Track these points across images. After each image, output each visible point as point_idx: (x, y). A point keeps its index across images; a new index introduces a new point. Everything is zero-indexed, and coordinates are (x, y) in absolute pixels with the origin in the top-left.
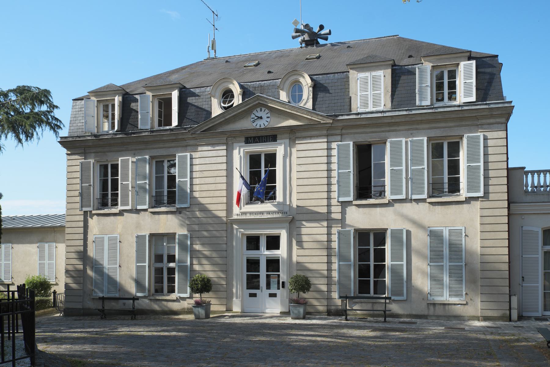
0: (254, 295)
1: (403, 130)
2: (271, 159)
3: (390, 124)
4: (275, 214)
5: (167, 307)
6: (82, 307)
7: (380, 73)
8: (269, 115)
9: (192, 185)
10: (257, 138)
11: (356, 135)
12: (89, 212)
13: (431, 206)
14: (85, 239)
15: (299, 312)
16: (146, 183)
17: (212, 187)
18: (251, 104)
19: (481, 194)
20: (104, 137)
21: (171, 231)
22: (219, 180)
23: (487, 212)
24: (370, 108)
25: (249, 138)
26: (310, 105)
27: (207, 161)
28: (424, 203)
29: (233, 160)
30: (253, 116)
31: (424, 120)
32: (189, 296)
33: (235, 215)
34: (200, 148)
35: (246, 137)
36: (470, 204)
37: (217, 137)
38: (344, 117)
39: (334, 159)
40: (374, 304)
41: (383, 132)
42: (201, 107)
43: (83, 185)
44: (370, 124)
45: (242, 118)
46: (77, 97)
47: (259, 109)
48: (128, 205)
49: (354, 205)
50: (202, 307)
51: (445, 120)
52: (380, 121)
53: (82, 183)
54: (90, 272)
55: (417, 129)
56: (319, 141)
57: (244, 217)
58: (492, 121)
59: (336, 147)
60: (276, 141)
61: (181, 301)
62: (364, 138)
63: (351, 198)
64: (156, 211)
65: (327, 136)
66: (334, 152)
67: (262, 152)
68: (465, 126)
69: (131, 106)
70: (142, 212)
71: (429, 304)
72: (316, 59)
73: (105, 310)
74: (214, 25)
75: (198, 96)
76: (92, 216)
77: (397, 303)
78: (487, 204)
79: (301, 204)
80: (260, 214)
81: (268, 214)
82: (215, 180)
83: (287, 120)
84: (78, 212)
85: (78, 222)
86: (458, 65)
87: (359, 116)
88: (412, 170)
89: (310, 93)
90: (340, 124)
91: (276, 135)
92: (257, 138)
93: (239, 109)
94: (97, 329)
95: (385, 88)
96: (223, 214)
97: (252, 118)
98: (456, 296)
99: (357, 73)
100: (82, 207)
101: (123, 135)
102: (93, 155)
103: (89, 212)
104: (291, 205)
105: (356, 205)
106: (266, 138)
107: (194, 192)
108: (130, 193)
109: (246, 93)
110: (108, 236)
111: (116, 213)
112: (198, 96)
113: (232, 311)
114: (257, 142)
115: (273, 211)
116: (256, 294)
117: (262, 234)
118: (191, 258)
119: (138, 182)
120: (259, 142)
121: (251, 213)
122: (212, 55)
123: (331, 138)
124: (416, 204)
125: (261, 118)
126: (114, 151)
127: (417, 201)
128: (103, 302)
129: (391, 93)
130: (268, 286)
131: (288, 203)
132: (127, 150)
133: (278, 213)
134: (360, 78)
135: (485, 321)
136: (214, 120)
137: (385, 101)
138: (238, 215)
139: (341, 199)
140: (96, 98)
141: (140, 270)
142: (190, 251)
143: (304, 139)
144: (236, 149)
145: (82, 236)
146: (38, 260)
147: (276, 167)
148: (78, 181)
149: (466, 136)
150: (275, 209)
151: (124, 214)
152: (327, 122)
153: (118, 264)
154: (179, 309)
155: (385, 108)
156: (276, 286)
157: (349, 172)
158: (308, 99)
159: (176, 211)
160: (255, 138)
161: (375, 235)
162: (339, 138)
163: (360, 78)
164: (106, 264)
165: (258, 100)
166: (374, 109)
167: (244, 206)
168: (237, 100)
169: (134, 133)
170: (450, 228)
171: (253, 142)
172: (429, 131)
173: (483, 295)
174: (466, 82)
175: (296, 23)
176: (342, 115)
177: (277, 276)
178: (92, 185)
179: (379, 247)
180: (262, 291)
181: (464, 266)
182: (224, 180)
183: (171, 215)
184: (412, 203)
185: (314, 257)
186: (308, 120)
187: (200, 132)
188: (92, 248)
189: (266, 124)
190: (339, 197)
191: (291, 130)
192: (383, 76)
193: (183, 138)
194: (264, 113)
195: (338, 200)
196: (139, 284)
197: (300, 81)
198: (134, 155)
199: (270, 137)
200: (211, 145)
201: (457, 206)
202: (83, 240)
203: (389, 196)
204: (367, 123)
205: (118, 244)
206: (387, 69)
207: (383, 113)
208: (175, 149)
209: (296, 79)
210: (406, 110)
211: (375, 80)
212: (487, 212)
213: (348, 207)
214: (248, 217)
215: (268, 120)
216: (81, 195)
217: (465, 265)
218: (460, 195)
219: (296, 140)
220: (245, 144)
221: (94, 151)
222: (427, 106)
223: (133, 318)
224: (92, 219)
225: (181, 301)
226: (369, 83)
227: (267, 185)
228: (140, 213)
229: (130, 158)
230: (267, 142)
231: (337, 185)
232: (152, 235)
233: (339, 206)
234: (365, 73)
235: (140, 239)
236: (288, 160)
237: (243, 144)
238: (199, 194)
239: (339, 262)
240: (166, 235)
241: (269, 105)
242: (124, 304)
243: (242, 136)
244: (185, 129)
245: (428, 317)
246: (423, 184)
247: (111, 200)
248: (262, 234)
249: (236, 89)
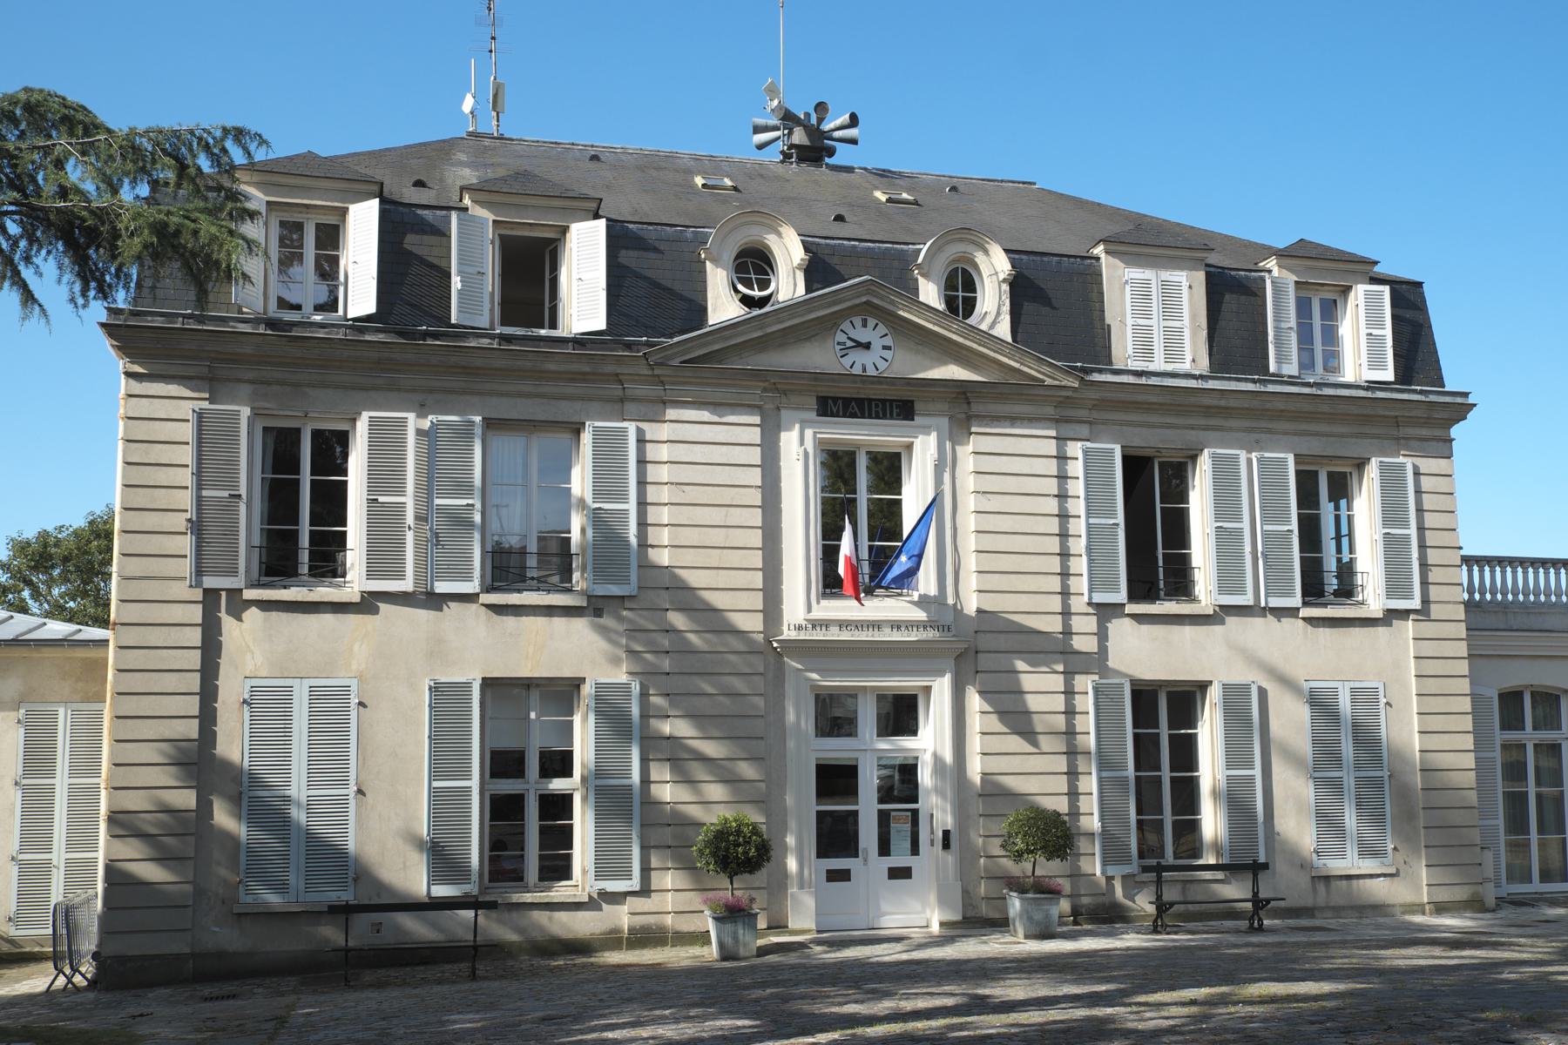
0: (843, 876)
1: (1285, 433)
3: (1208, 411)
4: (915, 629)
5: (541, 928)
6: (187, 950)
7: (1181, 277)
8: (888, 341)
9: (643, 524)
10: (853, 403)
11: (1124, 428)
12: (224, 594)
13: (1309, 627)
14: (208, 694)
15: (1048, 916)
16: (473, 505)
17: (717, 537)
18: (845, 301)
19: (1415, 603)
20: (312, 332)
21: (567, 673)
22: (738, 516)
23: (1429, 649)
24: (1158, 364)
25: (830, 401)
26: (1004, 330)
27: (698, 453)
28: (1293, 620)
29: (779, 460)
30: (840, 337)
31: (1288, 411)
32: (638, 889)
33: (792, 627)
34: (671, 413)
35: (820, 394)
36: (1391, 626)
37: (734, 386)
38: (1104, 376)
39: (1077, 488)
40: (1188, 886)
41: (1193, 428)
42: (669, 286)
43: (205, 493)
44: (1161, 404)
45: (808, 339)
47: (858, 321)
48: (400, 576)
49: (1129, 615)
50: (746, 920)
51: (1331, 418)
52: (1192, 400)
53: (200, 487)
54: (223, 818)
55: (1270, 431)
56: (1021, 433)
57: (819, 635)
58: (1424, 432)
59: (1080, 455)
60: (913, 420)
61: (604, 905)
62: (1146, 439)
63: (1121, 596)
64: (510, 603)
65: (1057, 421)
66: (1076, 468)
67: (858, 445)
68: (1372, 438)
69: (406, 241)
70: (452, 605)
71: (1316, 879)
72: (913, 204)
75: (656, 250)
76: (238, 606)
77: (1242, 880)
78: (1429, 629)
79: (991, 603)
80: (871, 629)
81: (895, 630)
82: (726, 516)
83: (945, 363)
84: (182, 590)
85: (178, 628)
86: (1346, 290)
87: (1143, 381)
88: (1265, 534)
89: (1003, 298)
90: (1093, 394)
91: (912, 402)
92: (853, 403)
93: (810, 311)
94: (726, 1019)
95: (1193, 317)
96: (752, 623)
97: (839, 343)
99: (1124, 266)
100: (199, 572)
101: (393, 335)
102: (246, 389)
103: (224, 594)
104: (959, 607)
105: (1134, 616)
106: (880, 406)
107: (650, 549)
108: (410, 536)
109: (818, 270)
110: (307, 683)
111: (348, 600)
112: (656, 250)
113: (787, 927)
115: (911, 621)
116: (911, 867)
117: (866, 687)
118: (645, 761)
119: (438, 501)
120: (859, 415)
121: (843, 624)
122: (491, 127)
123: (1068, 430)
124: (1276, 620)
125: (867, 346)
126: (337, 387)
127: (1280, 613)
129: (1206, 331)
130: (884, 849)
131: (950, 601)
132: (393, 387)
133: (925, 627)
134: (1132, 281)
135: (1440, 914)
136: (731, 331)
137: (1195, 352)
138: (800, 628)
139: (1099, 598)
140: (266, 195)
141: (445, 805)
142: (641, 738)
143: (995, 423)
144: (789, 429)
145: (194, 683)
147: (1319, 510)
148: (186, 477)
149: (1374, 462)
150: (920, 615)
151: (378, 607)
152: (1063, 384)
153: (352, 782)
154: (598, 931)
155: (1193, 367)
156: (908, 845)
157: (1114, 524)
158: (998, 314)
159: (585, 604)
160: (847, 401)
161: (1170, 695)
162: (1084, 430)
163: (1132, 281)
164: (298, 787)
165: (868, 292)
166: (1169, 368)
167: (818, 602)
168: (788, 285)
169: (436, 336)
170: (1353, 685)
171: (841, 413)
172: (1296, 438)
173: (1431, 849)
174: (1371, 334)
176: (1100, 371)
177: (909, 814)
178: (244, 496)
179: (1183, 731)
180: (866, 860)
181: (1386, 778)
182: (756, 517)
183: (563, 619)
184: (1266, 616)
185: (1030, 756)
186: (1001, 372)
187: (681, 363)
188: (239, 725)
189: (882, 365)
190: (1092, 592)
191: (961, 391)
192: (1187, 288)
193: (617, 375)
194: (873, 333)
195: (1090, 598)
196: (442, 860)
197: (976, 259)
198: (422, 412)
199: (873, 403)
200: (711, 407)
201: (1366, 629)
202: (198, 697)
204: (1160, 399)
205: (353, 715)
206: (1196, 270)
207: (1258, 385)
208: (578, 405)
209: (965, 252)
210: (1254, 381)
211: (1168, 291)
212: (1429, 649)
213: (1113, 621)
214: (834, 634)
215: (888, 354)
216: (197, 528)
217: (1390, 776)
219: (973, 422)
220: (818, 415)
221: (251, 375)
222: (1290, 377)
224: (240, 619)
225: (604, 905)
226: (1154, 297)
228: (445, 607)
229: (411, 416)
230: (884, 417)
231: (1085, 558)
232: (487, 683)
233: (1090, 617)
234: (1142, 270)
235: (445, 697)
236: (947, 477)
237: (813, 415)
238: (670, 558)
239: (1101, 771)
240: (538, 686)
241: (901, 313)
242: (377, 928)
243: (810, 391)
244: (629, 346)
245: (1316, 913)
246: (1292, 570)
247: (310, 552)
248: (865, 688)
249: (788, 250)
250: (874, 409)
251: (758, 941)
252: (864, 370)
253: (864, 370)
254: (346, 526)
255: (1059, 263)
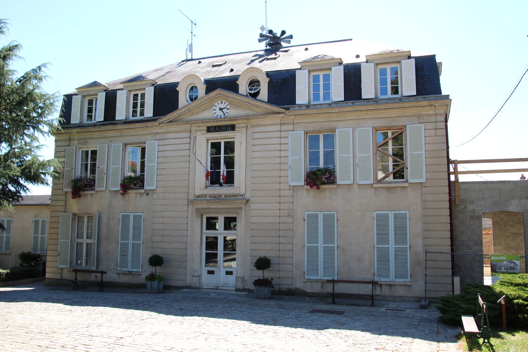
2: (230, 147)
25: (210, 128)
46: (73, 92)
73: (78, 282)
74: (192, 32)
92: (217, 128)
98: (402, 277)
114: (217, 131)
120: (219, 131)
128: (102, 275)
146: (33, 234)
147: (221, 155)
153: (142, 241)
170: (395, 212)
175: (262, 28)
181: (142, 244)
199: (229, 126)
203: (96, 189)
217: (410, 247)
218: (239, 187)
223: (101, 290)
227: (213, 170)
230: (226, 131)
250: (223, 128)
251: (502, 303)
252: (221, 117)
253: (221, 117)
254: (234, 169)
255: (291, 71)
